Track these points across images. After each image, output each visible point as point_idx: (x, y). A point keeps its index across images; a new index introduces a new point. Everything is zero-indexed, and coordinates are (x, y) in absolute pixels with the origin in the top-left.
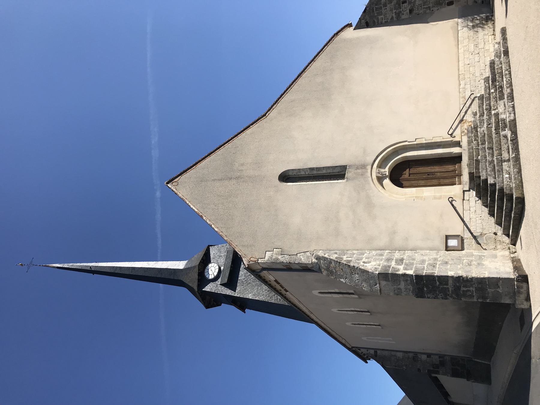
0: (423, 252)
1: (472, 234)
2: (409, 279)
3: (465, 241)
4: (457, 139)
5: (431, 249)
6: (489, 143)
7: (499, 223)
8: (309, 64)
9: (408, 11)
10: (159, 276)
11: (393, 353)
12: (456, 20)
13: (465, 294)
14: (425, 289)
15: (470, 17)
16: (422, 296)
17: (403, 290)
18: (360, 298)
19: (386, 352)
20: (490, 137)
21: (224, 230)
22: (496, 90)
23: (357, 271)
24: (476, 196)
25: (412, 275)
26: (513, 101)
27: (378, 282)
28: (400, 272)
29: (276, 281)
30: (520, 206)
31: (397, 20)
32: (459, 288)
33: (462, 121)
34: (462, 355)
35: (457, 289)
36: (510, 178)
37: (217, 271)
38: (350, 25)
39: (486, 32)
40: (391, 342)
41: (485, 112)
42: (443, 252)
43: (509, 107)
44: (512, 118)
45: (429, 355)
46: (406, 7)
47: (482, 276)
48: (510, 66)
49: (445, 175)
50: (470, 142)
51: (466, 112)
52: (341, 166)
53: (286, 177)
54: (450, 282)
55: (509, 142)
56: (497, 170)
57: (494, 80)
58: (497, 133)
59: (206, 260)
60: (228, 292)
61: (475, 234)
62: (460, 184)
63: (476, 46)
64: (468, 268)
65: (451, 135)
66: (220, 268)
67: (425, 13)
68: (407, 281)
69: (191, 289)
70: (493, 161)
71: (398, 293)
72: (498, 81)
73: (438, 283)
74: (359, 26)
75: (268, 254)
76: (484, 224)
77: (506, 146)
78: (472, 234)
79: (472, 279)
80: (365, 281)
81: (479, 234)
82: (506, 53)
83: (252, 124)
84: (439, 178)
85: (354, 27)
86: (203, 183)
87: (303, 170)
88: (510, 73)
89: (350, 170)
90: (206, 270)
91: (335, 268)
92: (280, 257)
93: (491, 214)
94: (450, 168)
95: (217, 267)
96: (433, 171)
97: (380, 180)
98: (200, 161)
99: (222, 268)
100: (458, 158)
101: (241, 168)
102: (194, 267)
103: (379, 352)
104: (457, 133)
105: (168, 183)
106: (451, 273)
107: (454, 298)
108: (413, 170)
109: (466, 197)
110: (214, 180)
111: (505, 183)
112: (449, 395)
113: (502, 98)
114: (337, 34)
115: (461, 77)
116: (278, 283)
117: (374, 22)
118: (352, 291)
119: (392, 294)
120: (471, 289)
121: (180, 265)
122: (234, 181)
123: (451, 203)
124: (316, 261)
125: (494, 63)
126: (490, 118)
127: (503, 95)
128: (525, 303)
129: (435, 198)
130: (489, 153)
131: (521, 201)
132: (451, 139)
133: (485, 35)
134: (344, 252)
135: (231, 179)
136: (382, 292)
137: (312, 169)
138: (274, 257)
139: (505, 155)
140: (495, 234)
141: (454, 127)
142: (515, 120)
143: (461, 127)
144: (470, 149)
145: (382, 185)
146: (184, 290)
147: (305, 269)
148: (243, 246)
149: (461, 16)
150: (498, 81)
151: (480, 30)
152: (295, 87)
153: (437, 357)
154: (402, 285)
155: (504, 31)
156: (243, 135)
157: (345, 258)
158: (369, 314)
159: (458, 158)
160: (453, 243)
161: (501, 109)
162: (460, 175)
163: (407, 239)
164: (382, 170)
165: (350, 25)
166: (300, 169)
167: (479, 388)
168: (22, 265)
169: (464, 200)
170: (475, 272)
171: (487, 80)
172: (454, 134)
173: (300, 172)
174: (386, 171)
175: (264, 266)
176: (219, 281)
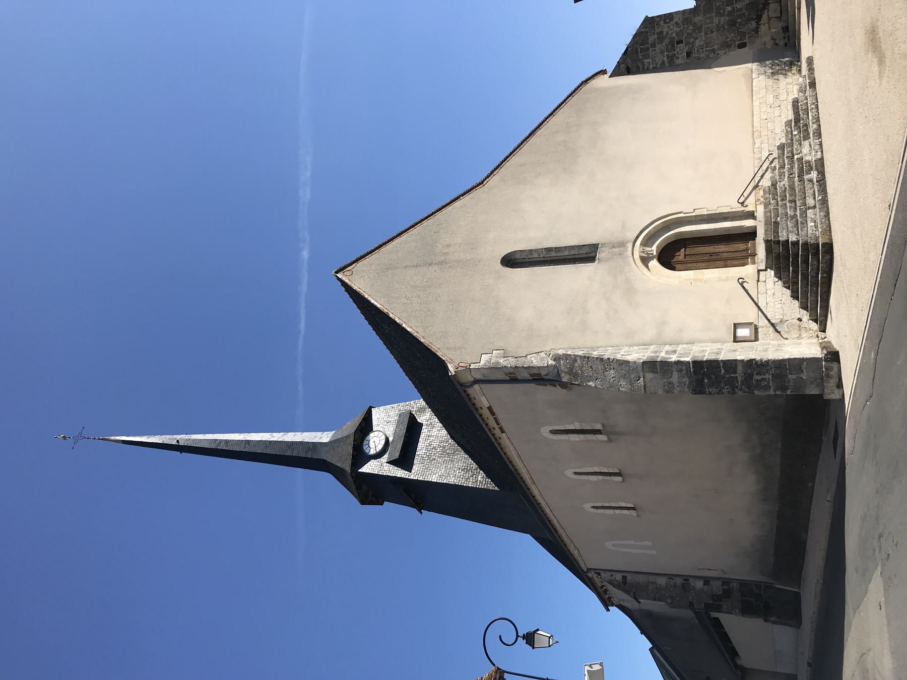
0: (703, 345)
1: (769, 320)
2: (684, 368)
3: (760, 330)
4: (751, 208)
6: (791, 195)
7: (804, 307)
8: (546, 119)
9: (685, 54)
10: (289, 453)
11: (651, 578)
12: (750, 65)
13: (758, 386)
14: (706, 381)
15: (768, 62)
17: (676, 384)
18: (610, 440)
20: (792, 188)
21: (420, 330)
22: (800, 132)
23: (614, 365)
24: (775, 276)
25: (688, 362)
26: (820, 137)
27: (641, 375)
28: (673, 360)
29: (490, 408)
30: (828, 257)
31: (670, 65)
32: (751, 376)
33: (756, 186)
34: (757, 577)
35: (748, 377)
36: (816, 227)
37: (383, 442)
38: (604, 72)
39: (789, 80)
40: (649, 552)
41: (786, 162)
42: (731, 345)
43: (815, 144)
44: (819, 156)
45: (707, 581)
46: (682, 49)
47: (781, 358)
48: (817, 99)
49: (734, 255)
50: (766, 205)
51: (762, 176)
53: (510, 261)
54: (740, 368)
55: (815, 186)
58: (801, 179)
59: (366, 426)
60: (400, 473)
61: (773, 321)
62: (754, 263)
63: (776, 97)
64: (764, 353)
65: (742, 203)
66: (387, 439)
67: (708, 57)
68: (681, 371)
71: (669, 389)
72: (803, 121)
73: (723, 371)
74: (617, 73)
76: (785, 309)
77: (811, 191)
78: (769, 320)
79: (768, 362)
81: (778, 321)
82: (813, 85)
83: (463, 195)
85: (609, 74)
86: (390, 272)
87: (536, 250)
88: (817, 107)
90: (365, 442)
91: (581, 368)
92: (501, 361)
93: (795, 296)
94: (741, 246)
95: (384, 437)
96: (718, 250)
97: (645, 261)
99: (391, 439)
100: (751, 234)
101: (445, 251)
103: (629, 577)
105: (337, 272)
106: (739, 358)
107: (744, 392)
108: (689, 251)
109: (762, 278)
110: (406, 267)
111: (810, 232)
112: (738, 655)
113: (806, 137)
116: (493, 414)
117: (638, 67)
118: (599, 427)
119: (660, 392)
120: (767, 376)
121: (325, 437)
122: (436, 268)
123: (742, 284)
124: (554, 363)
125: (798, 102)
126: (792, 167)
127: (809, 134)
128: (836, 391)
129: (720, 280)
130: (790, 207)
131: (829, 248)
132: (743, 209)
133: (788, 84)
134: (593, 349)
135: (430, 264)
136: (647, 389)
137: (549, 250)
138: (493, 361)
139: (810, 202)
140: (800, 320)
141: (746, 194)
142: (822, 158)
143: (756, 194)
144: (767, 223)
145: (647, 267)
146: (327, 478)
147: (537, 377)
148: (448, 349)
149: (760, 58)
150: (803, 121)
151: (781, 77)
152: (526, 147)
153: (720, 583)
156: (449, 208)
157: (595, 353)
158: (619, 479)
159: (751, 234)
160: (743, 332)
161: (805, 149)
162: (754, 255)
163: (681, 330)
165: (604, 72)
166: (531, 250)
167: (782, 634)
168: (64, 438)
169: (758, 281)
170: (772, 355)
172: (746, 203)
173: (531, 254)
174: (654, 249)
175: (478, 376)
176: (385, 458)
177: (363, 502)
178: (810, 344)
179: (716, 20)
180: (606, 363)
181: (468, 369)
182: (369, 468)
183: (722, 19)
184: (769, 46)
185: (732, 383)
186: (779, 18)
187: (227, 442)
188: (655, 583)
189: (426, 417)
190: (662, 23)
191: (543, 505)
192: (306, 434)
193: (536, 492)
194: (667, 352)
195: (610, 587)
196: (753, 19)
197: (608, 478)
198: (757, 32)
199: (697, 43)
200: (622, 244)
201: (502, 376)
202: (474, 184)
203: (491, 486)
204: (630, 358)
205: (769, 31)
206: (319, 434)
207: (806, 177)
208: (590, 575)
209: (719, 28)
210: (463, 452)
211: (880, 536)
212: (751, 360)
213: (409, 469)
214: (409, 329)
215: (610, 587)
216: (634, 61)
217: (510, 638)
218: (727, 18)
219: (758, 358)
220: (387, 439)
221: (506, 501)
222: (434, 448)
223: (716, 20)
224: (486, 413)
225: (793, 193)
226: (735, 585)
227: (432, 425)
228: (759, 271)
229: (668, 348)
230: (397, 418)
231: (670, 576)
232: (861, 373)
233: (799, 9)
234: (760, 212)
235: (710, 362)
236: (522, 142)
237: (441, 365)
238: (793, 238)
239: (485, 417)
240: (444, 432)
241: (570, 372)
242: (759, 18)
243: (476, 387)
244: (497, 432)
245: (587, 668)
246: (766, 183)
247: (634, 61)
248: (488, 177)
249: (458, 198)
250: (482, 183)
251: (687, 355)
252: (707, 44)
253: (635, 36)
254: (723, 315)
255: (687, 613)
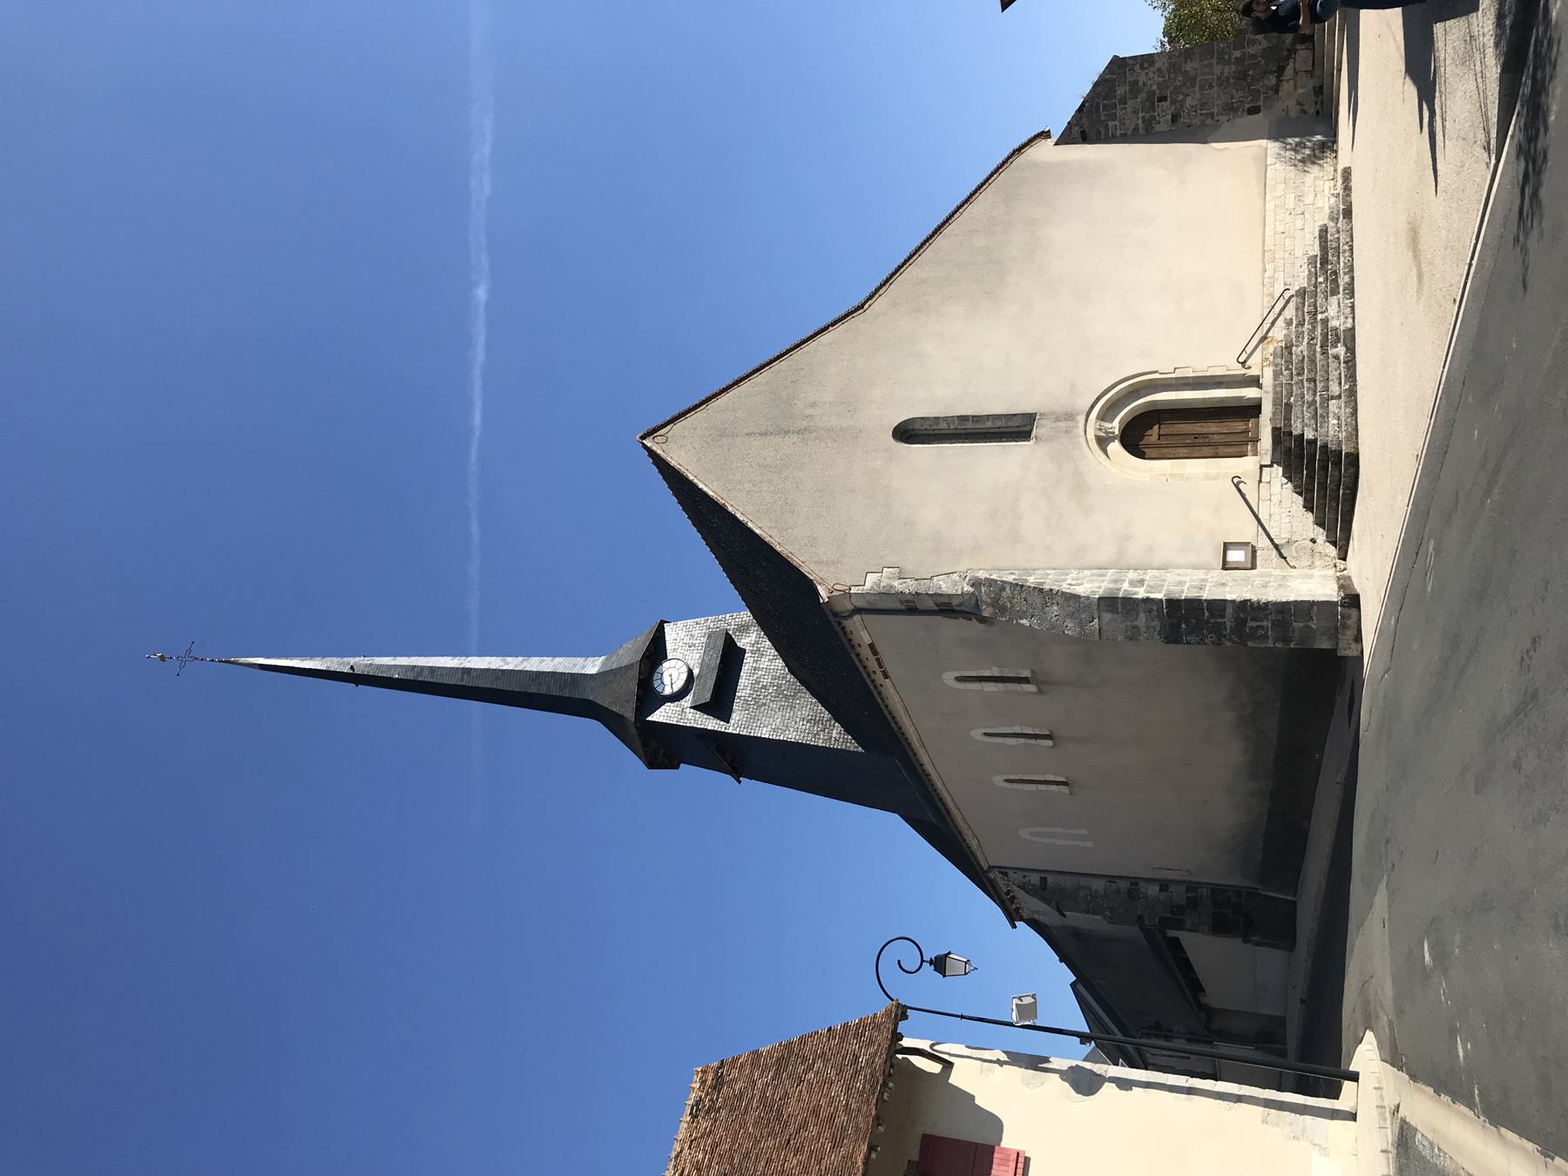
0: (1181, 571)
4: (1254, 371)
5: (1195, 567)
6: (1310, 371)
7: (1320, 523)
8: (959, 208)
10: (533, 689)
11: (1083, 881)
13: (1253, 635)
15: (1290, 140)
16: (1177, 641)
19: (1067, 878)
20: (1313, 361)
21: (774, 533)
28: (1140, 596)
29: (872, 646)
30: (1352, 470)
31: (1146, 133)
32: (1244, 622)
33: (1264, 338)
34: (1236, 881)
35: (1240, 623)
36: (1339, 426)
37: (684, 676)
38: (1045, 135)
40: (1082, 844)
42: (1219, 574)
44: (1349, 325)
45: (1164, 885)
46: (1166, 109)
49: (1229, 439)
50: (1277, 375)
51: (1273, 323)
52: (1023, 415)
53: (907, 433)
54: (1229, 611)
56: (1319, 417)
57: (1325, 261)
58: (1325, 353)
59: (656, 652)
60: (712, 724)
62: (1256, 454)
63: (1299, 198)
66: (690, 672)
67: (1203, 124)
68: (1150, 611)
69: (612, 722)
70: (1314, 401)
72: (1331, 264)
74: (1066, 139)
75: (871, 579)
80: (1071, 615)
82: (1348, 213)
83: (833, 324)
84: (1216, 445)
87: (945, 419)
89: (1043, 422)
90: (656, 676)
91: (1011, 599)
92: (896, 583)
93: (1308, 507)
94: (1239, 426)
95: (685, 669)
97: (1103, 442)
98: (716, 395)
99: (696, 672)
100: (1254, 409)
101: (808, 412)
102: (628, 667)
103: (1050, 879)
104: (1255, 361)
105: (643, 438)
106: (1229, 597)
108: (1165, 429)
109: (1265, 478)
113: (1335, 292)
114: (1019, 150)
115: (1267, 255)
116: (875, 653)
118: (1026, 673)
121: (592, 666)
122: (795, 438)
123: (1237, 486)
124: (972, 590)
126: (1314, 328)
128: (1353, 646)
129: (1207, 477)
131: (1354, 459)
132: (1243, 371)
135: (787, 432)
139: (1334, 389)
141: (1249, 349)
142: (1353, 328)
145: (1106, 452)
147: (946, 608)
149: (1277, 134)
150: (1331, 264)
152: (928, 253)
153: (1183, 889)
154: (1142, 621)
155: (1347, 174)
156: (812, 345)
158: (1050, 743)
159: (1254, 409)
160: (1236, 556)
161: (1332, 312)
162: (1256, 440)
164: (1107, 425)
165: (1045, 135)
166: (937, 418)
167: (1269, 960)
168: (162, 658)
170: (1273, 595)
171: (1312, 260)
174: (1115, 426)
175: (860, 604)
176: (688, 701)
177: (651, 765)
178: (1324, 577)
179: (1217, 70)
180: (1047, 596)
181: (847, 595)
182: (662, 715)
183: (1227, 69)
184: (1293, 114)
185: (1217, 630)
186: (1310, 73)
187: (432, 670)
188: (1089, 888)
189: (750, 638)
190: (1137, 68)
191: (934, 776)
192: (558, 660)
193: (924, 759)
194: (1132, 583)
195: (1020, 894)
196: (1272, 72)
197: (1033, 741)
198: (1277, 91)
199: (1189, 102)
200: (1070, 416)
201: (898, 606)
202: (850, 307)
203: (852, 745)
204: (1082, 590)
205: (1294, 91)
206: (580, 660)
207: (1332, 351)
208: (992, 875)
209: (1222, 82)
210: (808, 695)
211: (1388, 842)
212: (1245, 601)
213: (725, 716)
214: (757, 531)
215: (1011, 891)
216: (1090, 124)
217: (912, 962)
218: (1233, 68)
219: (1254, 599)
220: (690, 672)
221: (875, 765)
222: (764, 687)
223: (1217, 70)
224: (865, 652)
225: (1313, 369)
226: (1205, 892)
227: (759, 653)
228: (1262, 467)
229: (1132, 575)
230: (704, 640)
231: (1111, 879)
232: (1381, 632)
233: (1340, 70)
234: (1268, 380)
235: (1189, 601)
236: (923, 244)
237: (808, 587)
238: (1309, 435)
239: (863, 657)
240: (780, 663)
241: (995, 603)
242: (1280, 71)
243: (857, 618)
244: (879, 678)
245: (1015, 1001)
246: (1279, 333)
247: (1090, 124)
248: (871, 297)
249: (825, 329)
250: (862, 306)
251: (1158, 588)
252: (1203, 105)
253: (1096, 85)
254: (1205, 530)
255: (1132, 931)
